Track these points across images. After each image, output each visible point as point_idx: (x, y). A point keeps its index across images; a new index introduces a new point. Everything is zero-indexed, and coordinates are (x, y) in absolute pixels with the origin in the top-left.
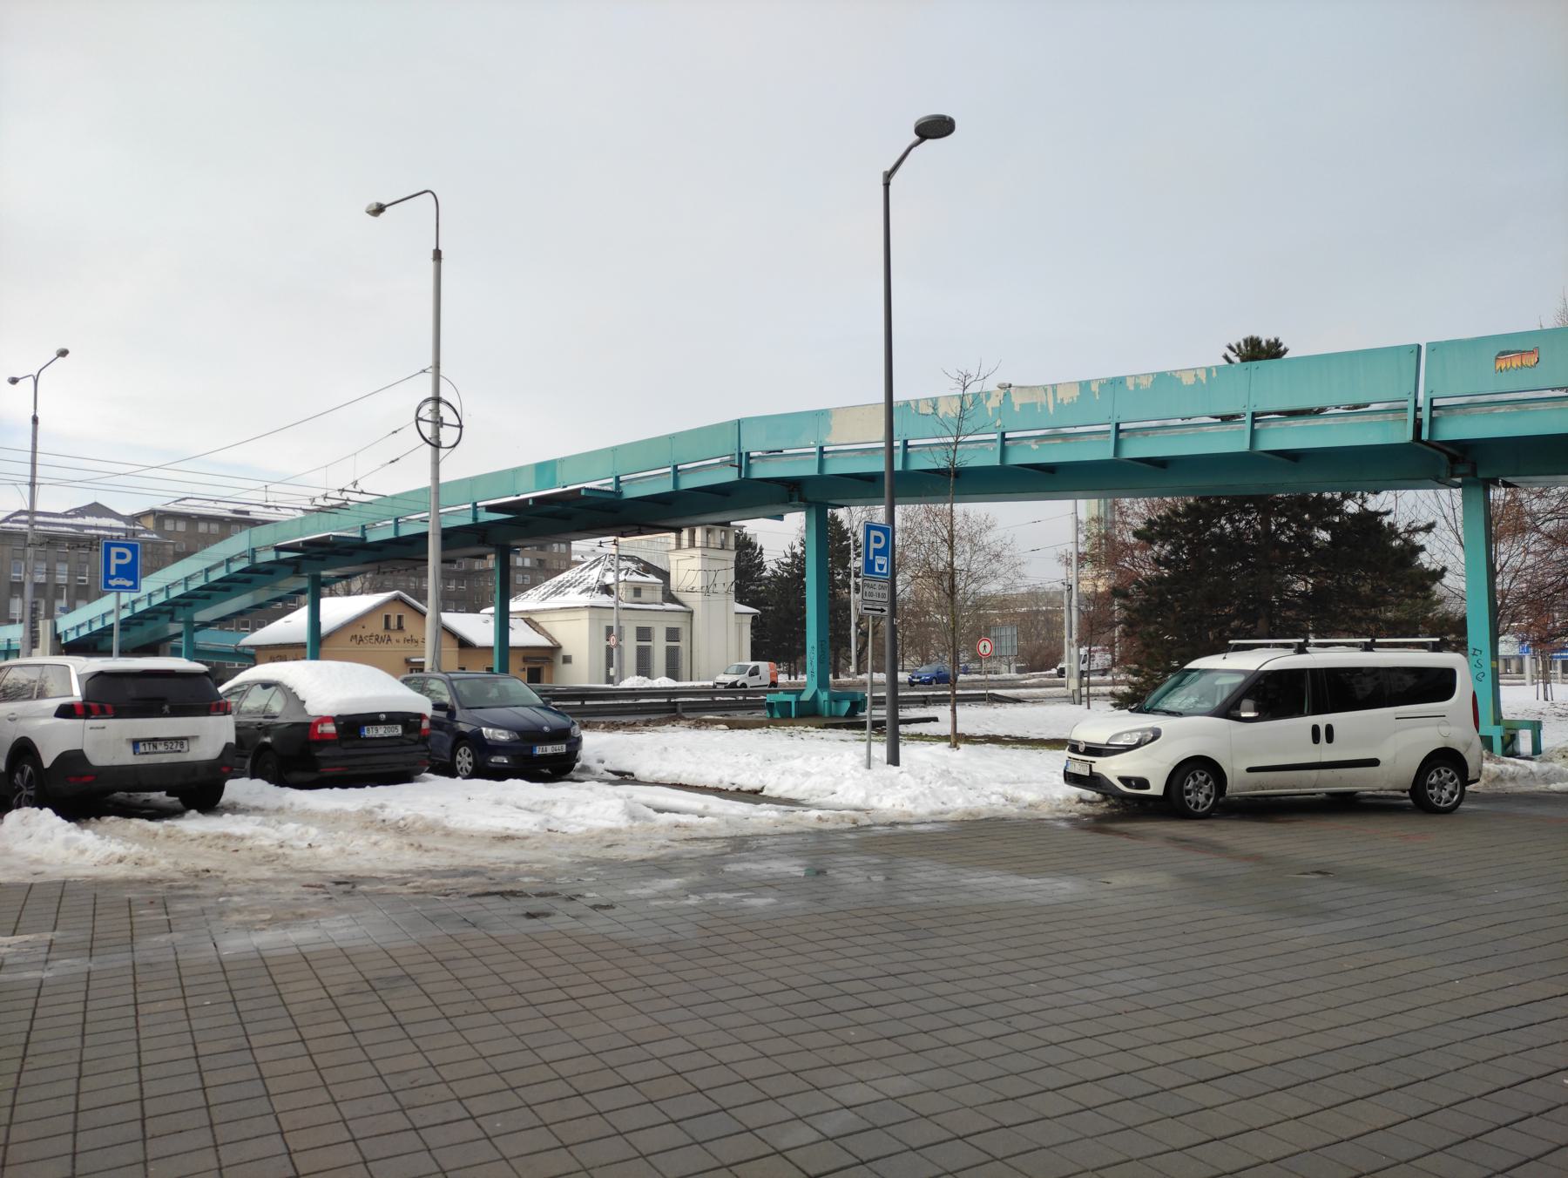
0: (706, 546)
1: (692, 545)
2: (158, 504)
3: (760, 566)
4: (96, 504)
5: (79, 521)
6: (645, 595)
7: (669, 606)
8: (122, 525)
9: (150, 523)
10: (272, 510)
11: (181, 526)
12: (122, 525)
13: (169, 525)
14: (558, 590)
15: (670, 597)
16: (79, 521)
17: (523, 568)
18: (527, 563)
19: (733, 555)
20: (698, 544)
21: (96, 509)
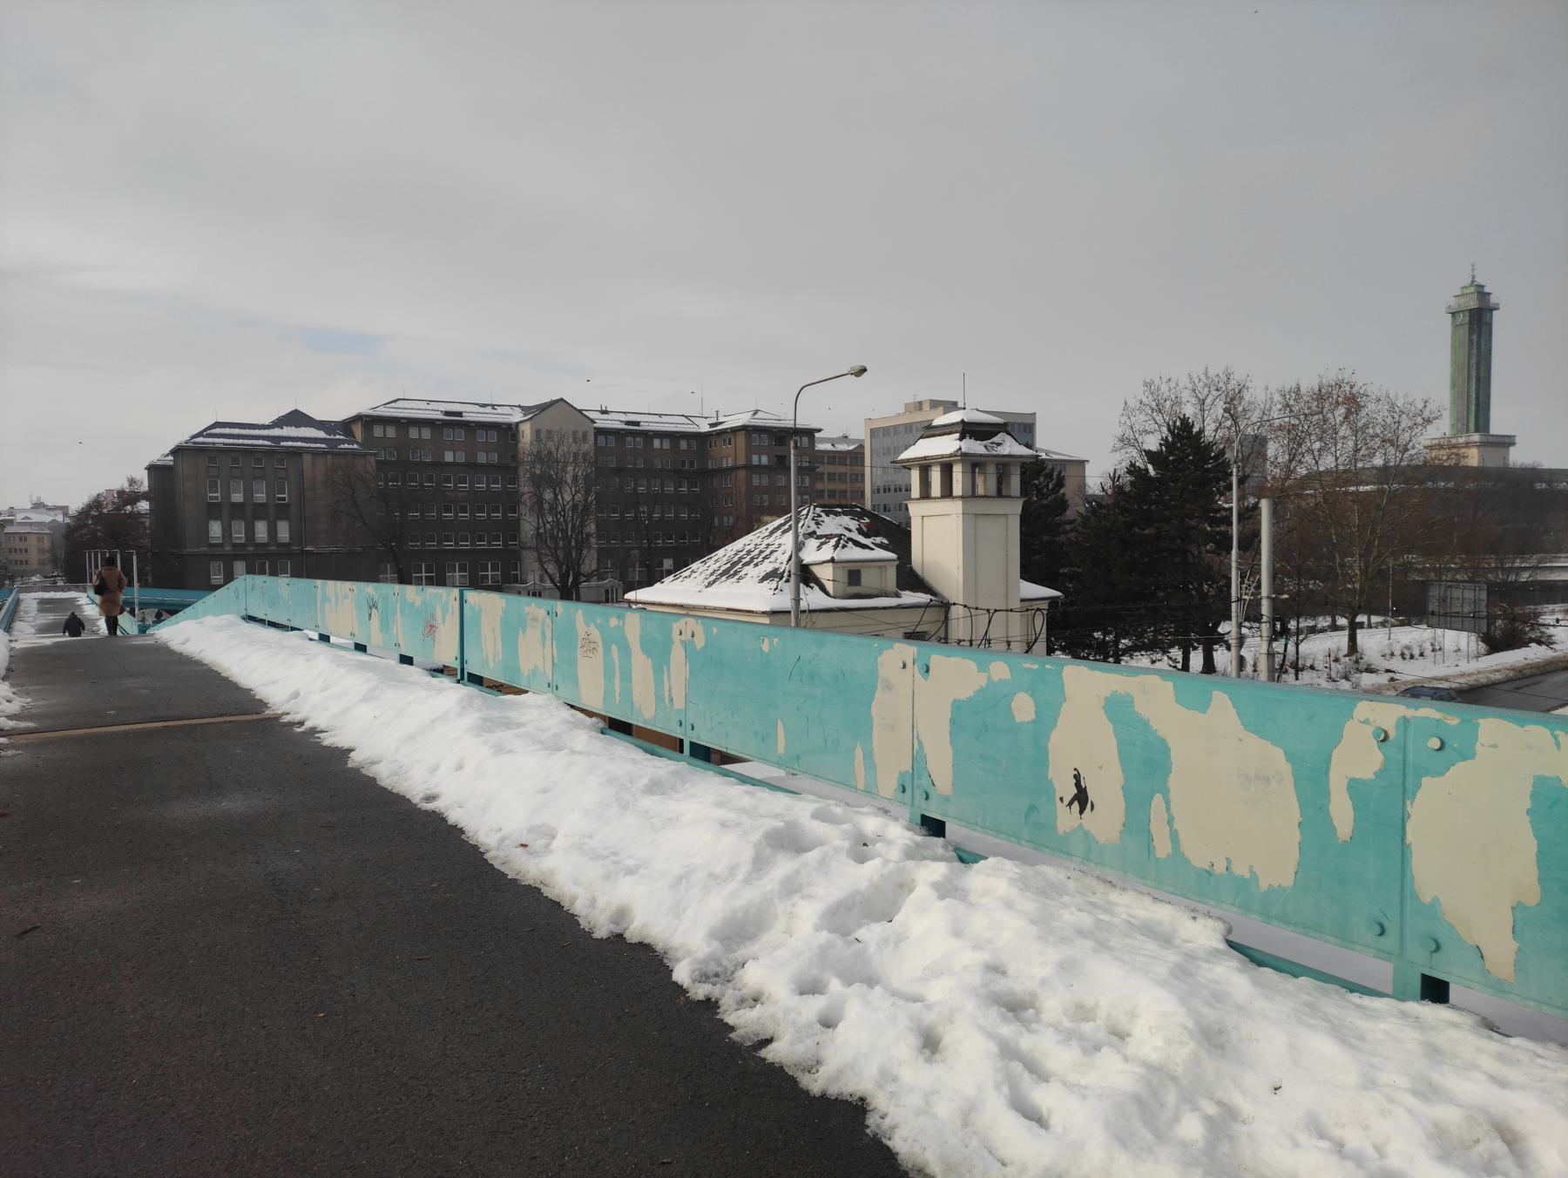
0: (971, 495)
1: (947, 493)
2: (364, 408)
3: (1063, 505)
4: (296, 412)
5: (276, 432)
6: (869, 579)
7: (909, 597)
8: (321, 434)
9: (358, 431)
10: (489, 409)
11: (391, 432)
12: (321, 434)
13: (378, 431)
14: (731, 572)
15: (910, 579)
16: (276, 432)
17: (760, 467)
18: (765, 460)
19: (1016, 508)
20: (957, 489)
21: (296, 418)
